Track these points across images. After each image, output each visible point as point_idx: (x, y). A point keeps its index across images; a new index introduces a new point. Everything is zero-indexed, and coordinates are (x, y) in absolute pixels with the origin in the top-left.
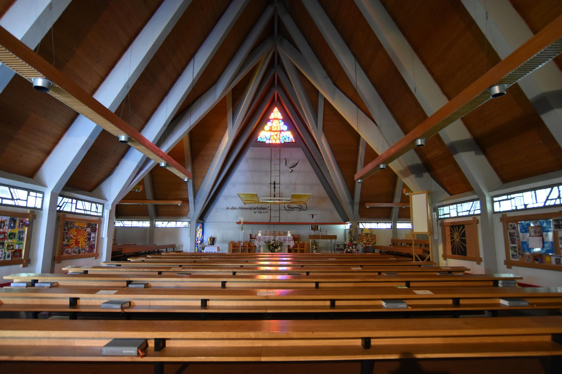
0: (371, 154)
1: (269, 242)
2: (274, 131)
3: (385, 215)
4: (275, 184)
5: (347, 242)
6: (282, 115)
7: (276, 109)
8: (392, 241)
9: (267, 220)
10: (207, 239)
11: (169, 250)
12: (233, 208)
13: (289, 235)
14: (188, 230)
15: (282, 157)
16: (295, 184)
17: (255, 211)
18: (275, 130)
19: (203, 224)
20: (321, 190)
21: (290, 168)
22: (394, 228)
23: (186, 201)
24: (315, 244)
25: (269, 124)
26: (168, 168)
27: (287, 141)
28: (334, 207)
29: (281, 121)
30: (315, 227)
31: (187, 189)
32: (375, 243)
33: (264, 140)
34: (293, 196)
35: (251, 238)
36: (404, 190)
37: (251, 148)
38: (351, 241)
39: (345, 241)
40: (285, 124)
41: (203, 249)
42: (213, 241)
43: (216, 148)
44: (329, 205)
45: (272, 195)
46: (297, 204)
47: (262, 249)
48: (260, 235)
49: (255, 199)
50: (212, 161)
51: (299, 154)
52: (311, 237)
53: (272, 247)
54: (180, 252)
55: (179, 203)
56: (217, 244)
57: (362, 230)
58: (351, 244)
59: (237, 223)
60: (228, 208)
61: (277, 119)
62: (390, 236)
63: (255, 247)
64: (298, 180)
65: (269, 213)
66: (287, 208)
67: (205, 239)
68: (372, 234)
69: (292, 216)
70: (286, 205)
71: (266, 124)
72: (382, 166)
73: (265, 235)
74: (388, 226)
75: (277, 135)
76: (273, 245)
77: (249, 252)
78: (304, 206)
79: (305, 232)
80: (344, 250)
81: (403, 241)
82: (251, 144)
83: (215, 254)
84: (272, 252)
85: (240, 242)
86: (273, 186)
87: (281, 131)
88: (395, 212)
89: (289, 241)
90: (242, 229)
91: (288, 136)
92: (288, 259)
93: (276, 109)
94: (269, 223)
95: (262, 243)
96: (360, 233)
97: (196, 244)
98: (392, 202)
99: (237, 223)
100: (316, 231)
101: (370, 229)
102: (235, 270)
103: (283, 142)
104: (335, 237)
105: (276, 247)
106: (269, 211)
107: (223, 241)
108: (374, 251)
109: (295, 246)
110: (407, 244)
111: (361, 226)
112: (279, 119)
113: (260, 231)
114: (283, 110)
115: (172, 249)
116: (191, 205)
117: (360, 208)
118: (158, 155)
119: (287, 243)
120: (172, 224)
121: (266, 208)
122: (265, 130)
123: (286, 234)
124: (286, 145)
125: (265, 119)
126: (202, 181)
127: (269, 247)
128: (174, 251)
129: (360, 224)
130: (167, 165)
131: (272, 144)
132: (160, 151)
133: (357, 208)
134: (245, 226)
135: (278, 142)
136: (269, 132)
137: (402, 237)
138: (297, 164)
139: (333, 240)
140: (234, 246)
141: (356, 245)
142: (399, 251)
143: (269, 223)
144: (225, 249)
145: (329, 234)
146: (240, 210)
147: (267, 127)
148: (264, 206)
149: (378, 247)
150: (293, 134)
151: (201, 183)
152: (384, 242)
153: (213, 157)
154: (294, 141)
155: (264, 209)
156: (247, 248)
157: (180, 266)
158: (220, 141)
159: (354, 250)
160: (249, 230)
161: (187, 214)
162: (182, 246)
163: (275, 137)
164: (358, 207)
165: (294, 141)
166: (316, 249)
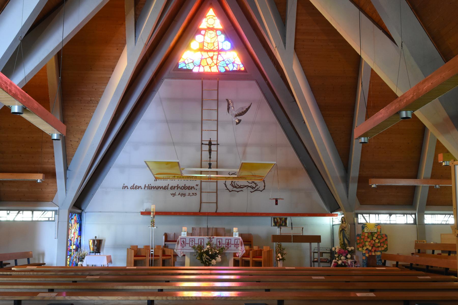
0: (381, 95)
1: (200, 247)
2: (207, 51)
3: (404, 200)
4: (210, 144)
5: (337, 247)
6: (223, 23)
7: (211, 12)
8: (417, 245)
10: (87, 243)
11: (20, 262)
12: (135, 187)
13: (236, 235)
14: (54, 225)
15: (222, 97)
16: (245, 145)
17: (173, 191)
18: (209, 48)
19: (80, 216)
20: (288, 156)
21: (236, 116)
22: (419, 223)
23: (51, 174)
24: (281, 250)
25: (199, 38)
26: (24, 116)
27: (231, 68)
29: (219, 33)
30: (280, 221)
31: (53, 153)
32: (386, 249)
33: (191, 67)
34: (243, 166)
35: (166, 241)
36: (440, 156)
37: (165, 80)
38: (343, 245)
39: (333, 245)
40: (227, 39)
41: (81, 259)
42: (98, 245)
43: (106, 80)
44: (305, 182)
45: (205, 164)
46: (248, 179)
47: (187, 260)
48: (184, 234)
49: (175, 171)
50: (98, 102)
51: (251, 92)
52: (276, 238)
53: (205, 257)
54: (40, 265)
55: (39, 178)
56: (106, 251)
57: (364, 226)
58: (344, 251)
59: (142, 213)
60: (125, 187)
61: (212, 29)
62: (412, 237)
63: (176, 256)
64: (247, 138)
66: (230, 188)
67: (83, 243)
68: (381, 234)
70: (229, 182)
71: (194, 38)
72: (404, 114)
73: (192, 235)
74: (410, 219)
75: (212, 58)
76: (207, 252)
77: (163, 265)
78: (260, 185)
79: (264, 228)
80: (331, 262)
81: (437, 245)
82: (166, 74)
83: (103, 269)
84: (206, 265)
85: (147, 247)
86: (206, 148)
87: (219, 51)
88: (421, 196)
89: (236, 245)
90: (153, 224)
91: (233, 60)
92: (232, 277)
93: (211, 12)
94: (199, 214)
95: (188, 249)
96: (359, 231)
97: (68, 250)
98: (415, 176)
99: (142, 213)
100: (283, 228)
101: (378, 225)
102: (151, 298)
103: (223, 70)
104: (317, 239)
105: (213, 257)
106: (198, 193)
107: (116, 246)
108: (384, 265)
109: (247, 255)
110: (443, 252)
111: (361, 219)
112: (217, 30)
113: (185, 229)
114: (223, 13)
115: (25, 261)
116: (60, 181)
117: (358, 188)
118: (9, 92)
120: (25, 216)
121: (192, 188)
122: (191, 50)
123: (230, 233)
124: (229, 76)
125: (191, 29)
126: (80, 139)
127: (201, 255)
128: (29, 264)
129: (360, 216)
130: (24, 109)
132: (11, 83)
133: (353, 187)
134: (158, 219)
135: (214, 70)
136: (199, 53)
137: (435, 239)
138: (247, 109)
139: (314, 245)
140: (137, 255)
141: (352, 252)
142: (429, 264)
143: (199, 214)
144: (121, 261)
145: (307, 233)
146: (147, 191)
147: (195, 43)
148: (189, 183)
149: (391, 257)
151: (78, 142)
152: (402, 247)
153: (100, 96)
154: (243, 69)
155: (190, 188)
156: (161, 258)
157: (51, 291)
158: (112, 68)
159: (349, 261)
160: (166, 226)
161: (53, 199)
162: (43, 254)
163: (209, 61)
164: (356, 185)
165: (243, 69)
166: (283, 259)
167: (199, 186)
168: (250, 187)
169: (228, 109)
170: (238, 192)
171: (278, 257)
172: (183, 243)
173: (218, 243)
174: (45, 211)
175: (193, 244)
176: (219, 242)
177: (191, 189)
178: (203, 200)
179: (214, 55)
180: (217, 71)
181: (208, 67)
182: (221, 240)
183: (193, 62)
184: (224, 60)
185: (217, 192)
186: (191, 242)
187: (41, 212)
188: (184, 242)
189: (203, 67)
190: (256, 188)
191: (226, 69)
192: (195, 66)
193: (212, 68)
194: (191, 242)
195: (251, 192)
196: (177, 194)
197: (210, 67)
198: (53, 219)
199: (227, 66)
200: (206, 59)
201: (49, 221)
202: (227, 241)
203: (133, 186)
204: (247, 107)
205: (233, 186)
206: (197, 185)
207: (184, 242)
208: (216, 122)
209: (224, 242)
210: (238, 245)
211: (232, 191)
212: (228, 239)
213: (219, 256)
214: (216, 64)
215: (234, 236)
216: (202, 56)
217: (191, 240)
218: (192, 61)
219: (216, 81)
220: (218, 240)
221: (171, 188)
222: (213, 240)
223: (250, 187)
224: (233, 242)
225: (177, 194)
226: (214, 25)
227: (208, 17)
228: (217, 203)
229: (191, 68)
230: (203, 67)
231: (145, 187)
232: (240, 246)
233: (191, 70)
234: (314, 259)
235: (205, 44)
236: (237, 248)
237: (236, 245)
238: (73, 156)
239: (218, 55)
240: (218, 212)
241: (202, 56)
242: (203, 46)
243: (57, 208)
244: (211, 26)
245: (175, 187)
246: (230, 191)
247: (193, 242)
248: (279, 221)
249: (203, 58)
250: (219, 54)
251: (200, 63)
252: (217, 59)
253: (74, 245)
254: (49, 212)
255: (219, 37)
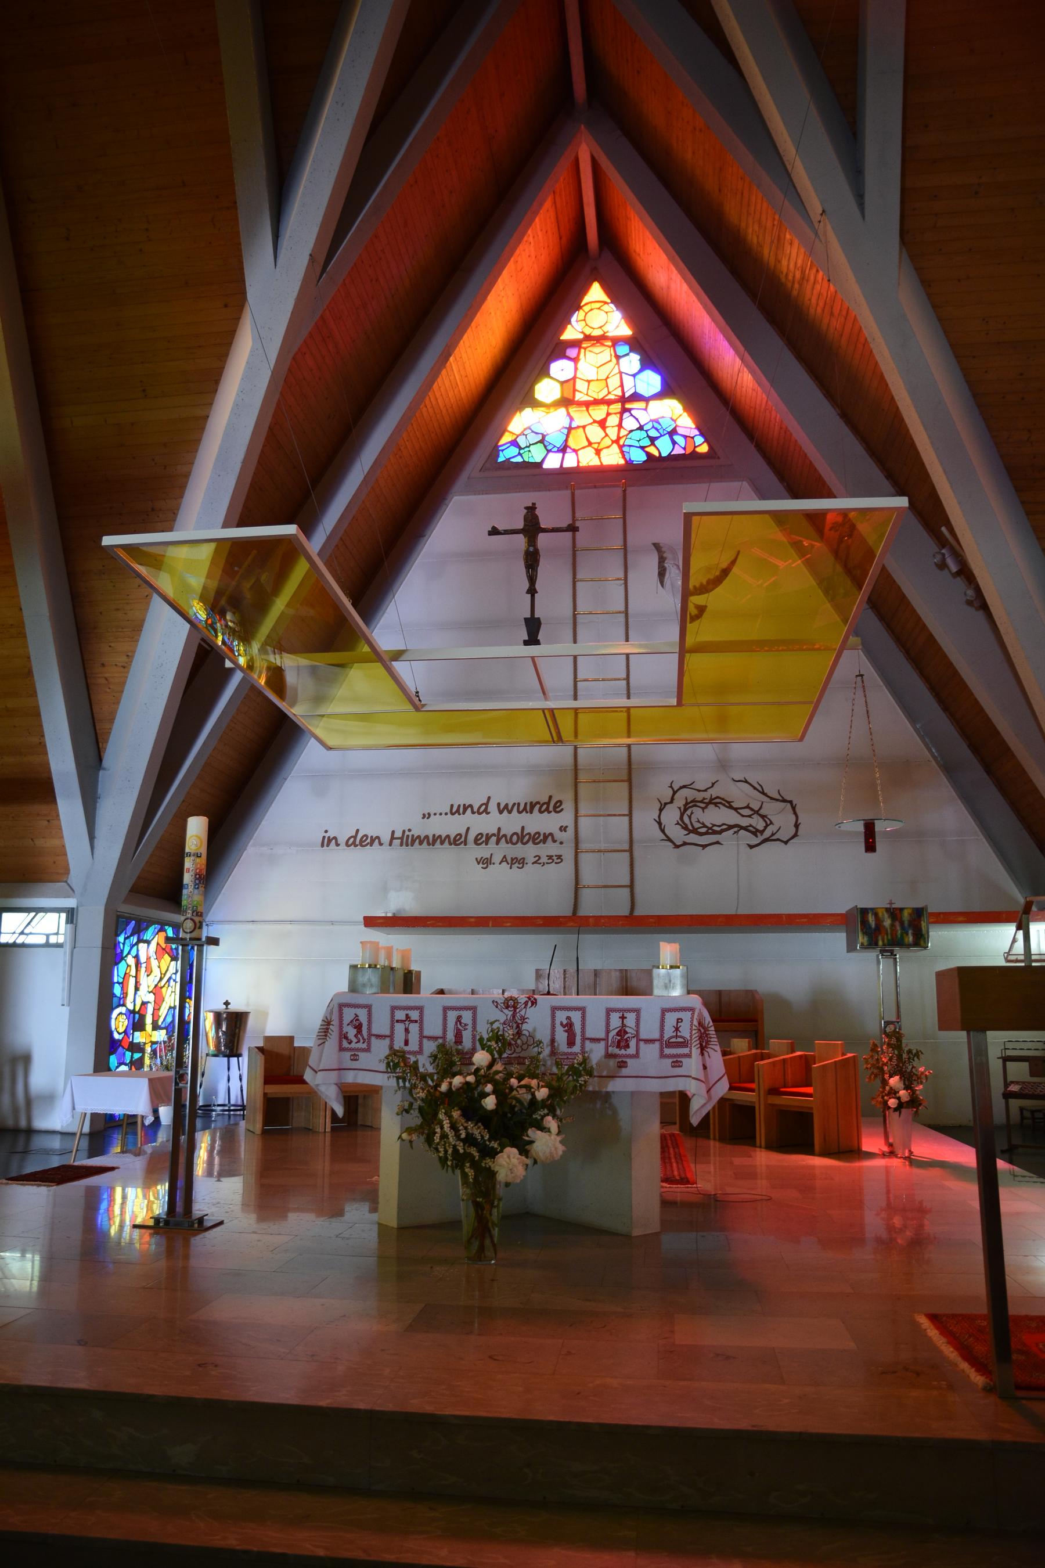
2: (587, 404)
7: (596, 292)
9: (558, 906)
12: (360, 841)
13: (671, 985)
14: (62, 957)
17: (483, 852)
18: (596, 401)
25: (560, 369)
27: (664, 447)
28: (971, 823)
33: (536, 454)
40: (647, 364)
58: (353, 988)
60: (328, 841)
61: (600, 340)
65: (567, 868)
66: (678, 834)
69: (713, 876)
70: (671, 816)
75: (602, 424)
78: (782, 821)
87: (627, 401)
91: (671, 421)
93: (596, 292)
94: (572, 922)
103: (638, 457)
106: (568, 853)
112: (616, 341)
116: (69, 808)
119: (648, 1074)
122: (535, 404)
124: (657, 472)
126: (130, 656)
131: (578, 472)
135: (612, 458)
138: (726, 572)
143: (572, 922)
147: (546, 390)
150: (691, 407)
151: (126, 667)
154: (704, 449)
162: (26, 1059)
163: (595, 433)
165: (704, 449)
167: (571, 831)
168: (745, 829)
169: (662, 574)
170: (704, 846)
171: (893, 1093)
172: (352, 1032)
173: (561, 1036)
174: (38, 910)
175: (414, 1037)
176: (569, 1026)
177: (544, 841)
178: (586, 878)
179: (608, 414)
180: (622, 462)
181: (590, 451)
182: (576, 1017)
183: (542, 441)
184: (641, 428)
185: (631, 850)
186: (399, 1028)
187: (23, 915)
188: (359, 1028)
189: (575, 451)
190: (767, 833)
191: (648, 454)
192: (549, 451)
193: (602, 453)
194: (399, 1028)
195: (751, 847)
196: (496, 859)
197: (598, 452)
198: (61, 939)
199: (653, 444)
200: (584, 427)
201: (47, 945)
202: (615, 1021)
203: (355, 837)
204: (724, 565)
205: (686, 828)
206: (563, 829)
207: (359, 1028)
208: (621, 618)
209: (595, 1027)
210: (684, 1044)
211: (685, 844)
212: (623, 1013)
213: (551, 1123)
214: (617, 441)
215: (657, 992)
216: (572, 419)
217: (400, 1015)
218: (540, 437)
219: (619, 491)
220: (561, 1016)
221: (476, 841)
222: (531, 1012)
223: (745, 829)
224: (649, 1028)
225: (496, 859)
226: (605, 329)
227: (586, 308)
228: (632, 886)
229: (539, 460)
230: (575, 451)
231: (393, 838)
232: (695, 1052)
233: (539, 465)
234: (1006, 1084)
235: (580, 385)
236: (677, 1064)
237: (671, 1045)
238: (112, 720)
239: (622, 413)
240: (637, 913)
241: (572, 419)
242: (575, 390)
243: (71, 903)
244: (597, 333)
245: (488, 837)
246: (677, 847)
247: (414, 1028)
248: (887, 923)
249: (574, 425)
250: (624, 410)
251: (566, 441)
252: (620, 426)
253: (156, 1027)
254: (49, 914)
255: (621, 360)
